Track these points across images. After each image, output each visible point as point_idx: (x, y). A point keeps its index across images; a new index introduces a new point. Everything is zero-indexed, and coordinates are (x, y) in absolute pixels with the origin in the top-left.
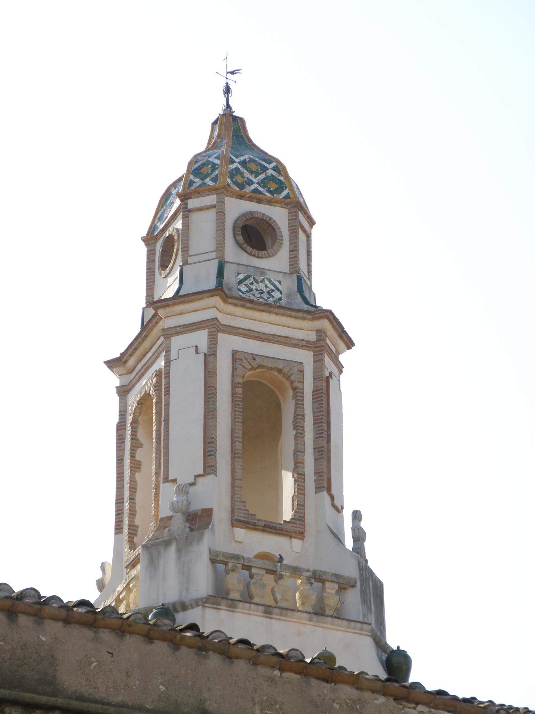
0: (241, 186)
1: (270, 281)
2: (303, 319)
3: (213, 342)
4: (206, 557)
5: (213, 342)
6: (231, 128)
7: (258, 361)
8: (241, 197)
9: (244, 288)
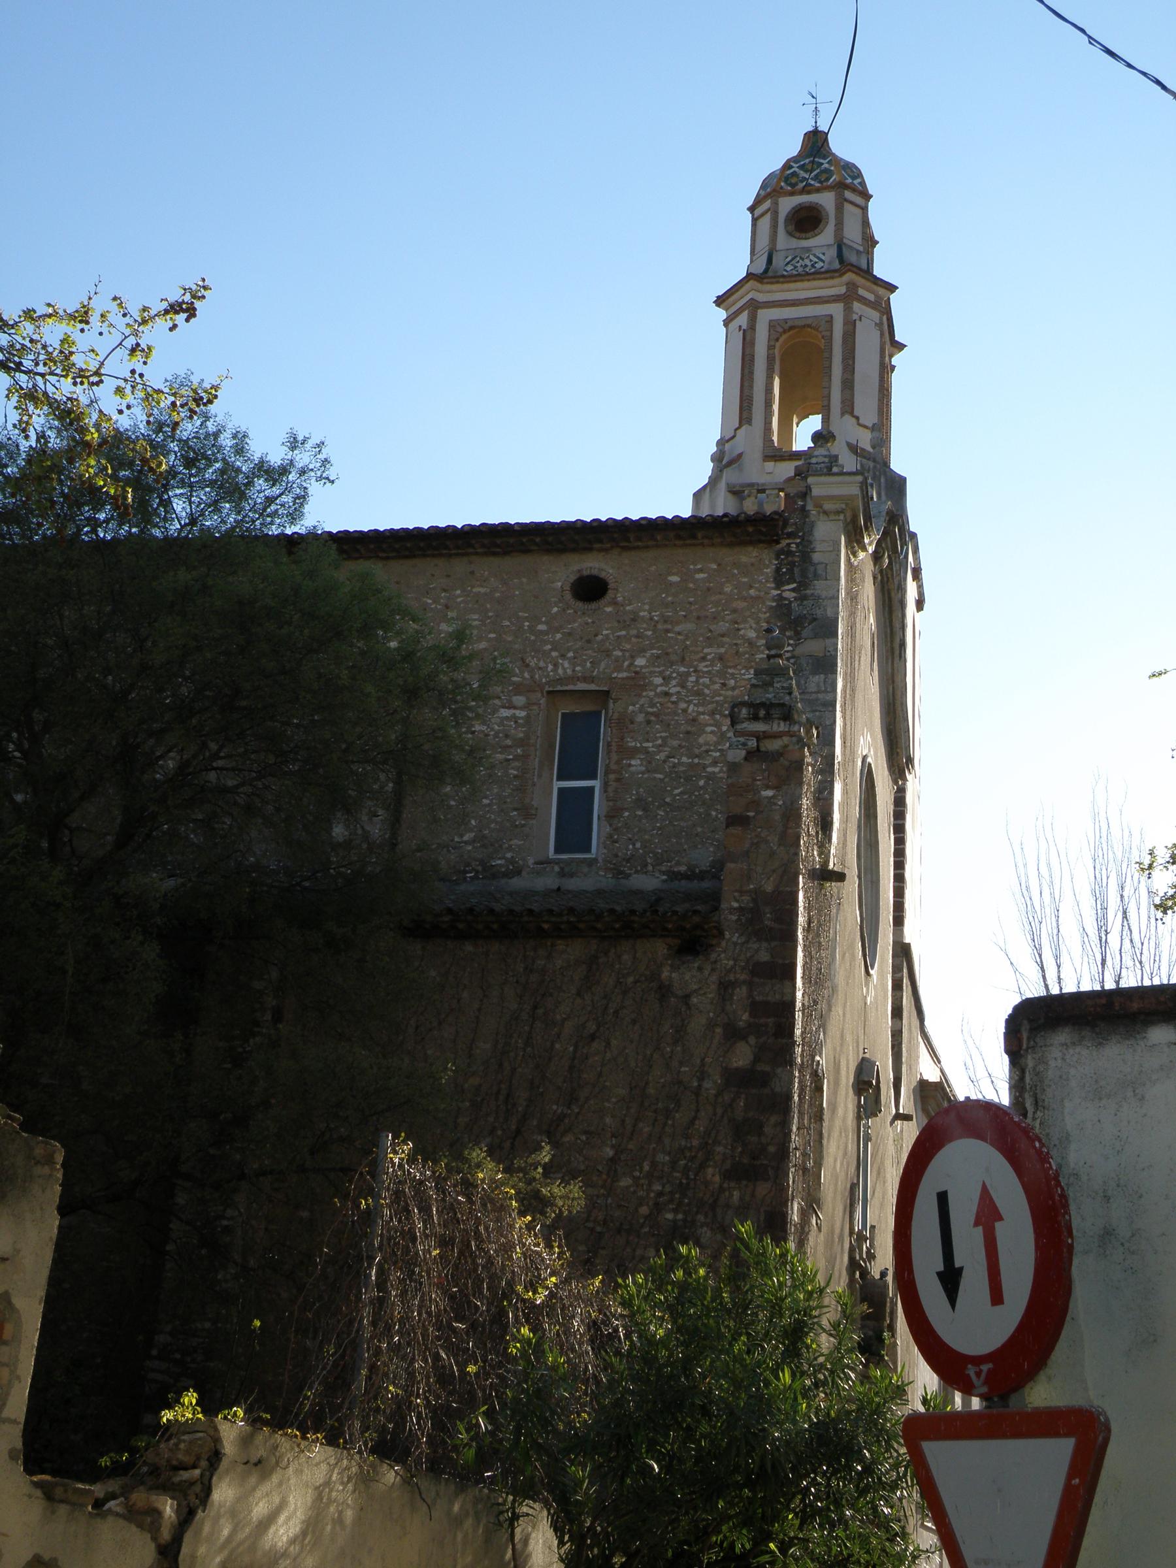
0: (793, 185)
1: (815, 255)
2: (832, 278)
3: (753, 320)
4: (846, 449)
5: (753, 320)
6: (816, 142)
7: (790, 324)
8: (792, 194)
9: (789, 268)
